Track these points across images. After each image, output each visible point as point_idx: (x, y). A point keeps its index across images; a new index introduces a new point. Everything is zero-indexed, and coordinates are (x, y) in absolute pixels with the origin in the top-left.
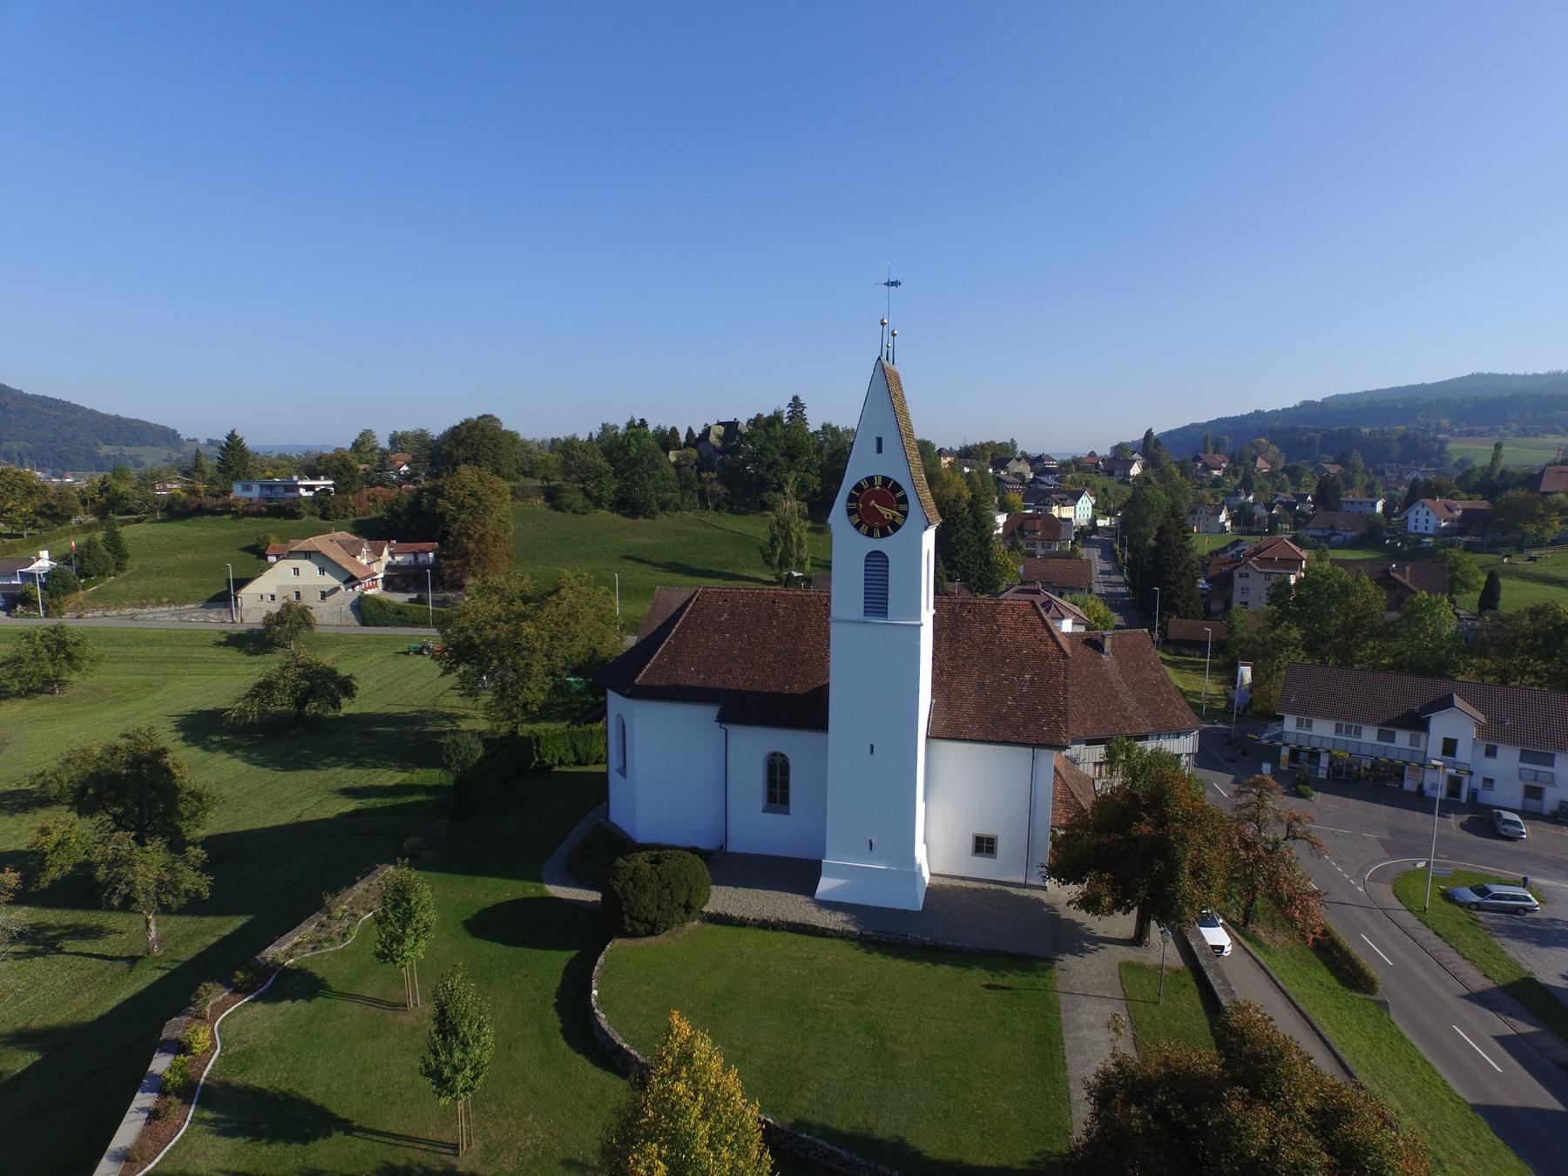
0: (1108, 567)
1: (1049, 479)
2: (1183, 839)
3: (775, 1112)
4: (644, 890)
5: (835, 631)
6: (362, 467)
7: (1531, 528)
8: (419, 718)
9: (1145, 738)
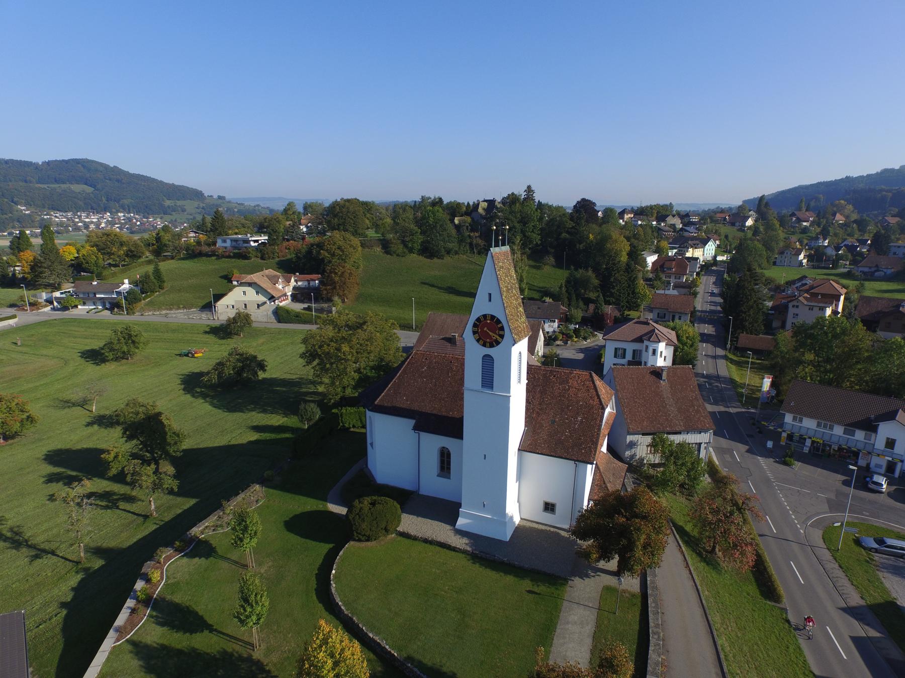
1: (691, 229)
2: (639, 529)
4: (363, 520)
5: (467, 396)
6: (288, 223)
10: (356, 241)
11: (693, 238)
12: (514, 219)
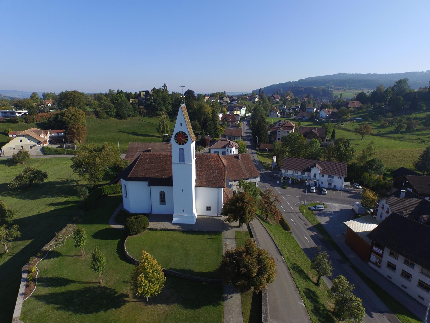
0: (248, 128)
1: (234, 103)
3: (165, 267)
4: (134, 225)
5: (174, 166)
6: (34, 104)
7: (345, 117)
8: (67, 182)
9: (248, 179)
10: (82, 112)
11: (236, 107)
12: (159, 99)
